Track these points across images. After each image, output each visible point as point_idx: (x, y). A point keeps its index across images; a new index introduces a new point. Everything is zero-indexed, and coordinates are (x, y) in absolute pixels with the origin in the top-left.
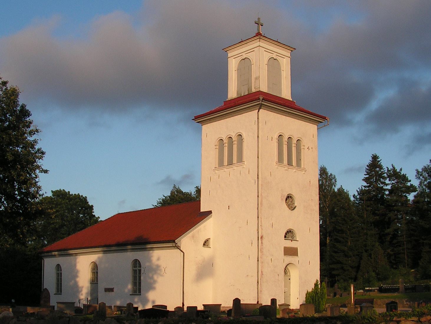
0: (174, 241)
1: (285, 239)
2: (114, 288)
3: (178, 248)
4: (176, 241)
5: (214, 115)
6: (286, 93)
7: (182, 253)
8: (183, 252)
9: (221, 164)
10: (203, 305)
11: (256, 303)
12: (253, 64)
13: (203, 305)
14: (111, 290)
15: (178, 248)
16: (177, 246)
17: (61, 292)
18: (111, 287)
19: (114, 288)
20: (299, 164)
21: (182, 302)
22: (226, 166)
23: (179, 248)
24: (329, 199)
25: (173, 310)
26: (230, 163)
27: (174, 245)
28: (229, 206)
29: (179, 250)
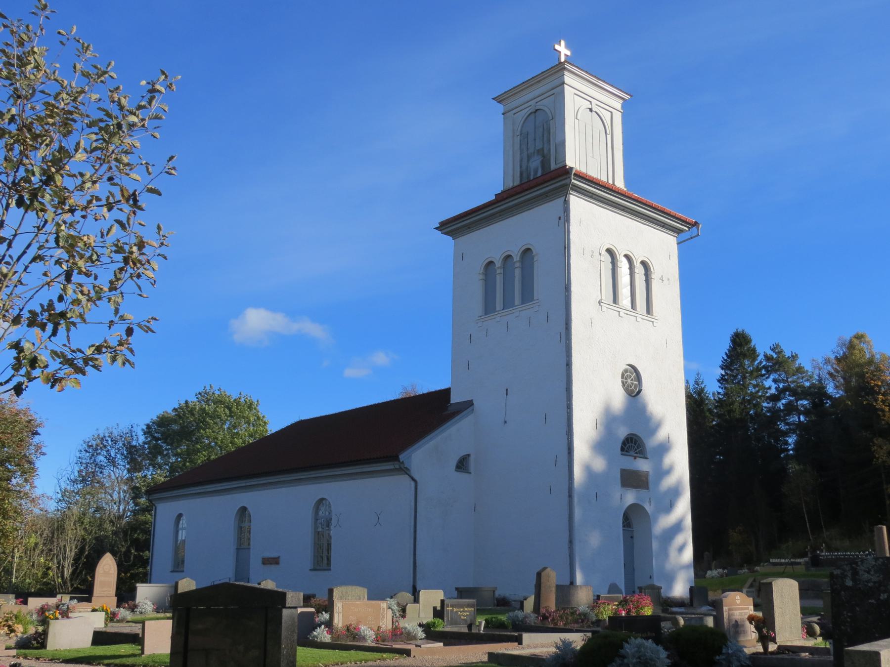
0: (396, 458)
1: (622, 454)
2: (279, 557)
3: (404, 470)
4: (400, 457)
5: (465, 220)
6: (620, 184)
7: (413, 483)
8: (413, 479)
9: (489, 308)
10: (457, 589)
11: (568, 583)
12: (517, 136)
13: (457, 589)
14: (275, 561)
15: (404, 470)
16: (403, 467)
17: (329, 564)
18: (274, 555)
19: (279, 557)
20: (649, 310)
21: (412, 584)
22: (500, 312)
23: (408, 472)
24: (179, 410)
25: (751, 599)
26: (508, 303)
27: (397, 467)
28: (507, 390)
29: (407, 476)
